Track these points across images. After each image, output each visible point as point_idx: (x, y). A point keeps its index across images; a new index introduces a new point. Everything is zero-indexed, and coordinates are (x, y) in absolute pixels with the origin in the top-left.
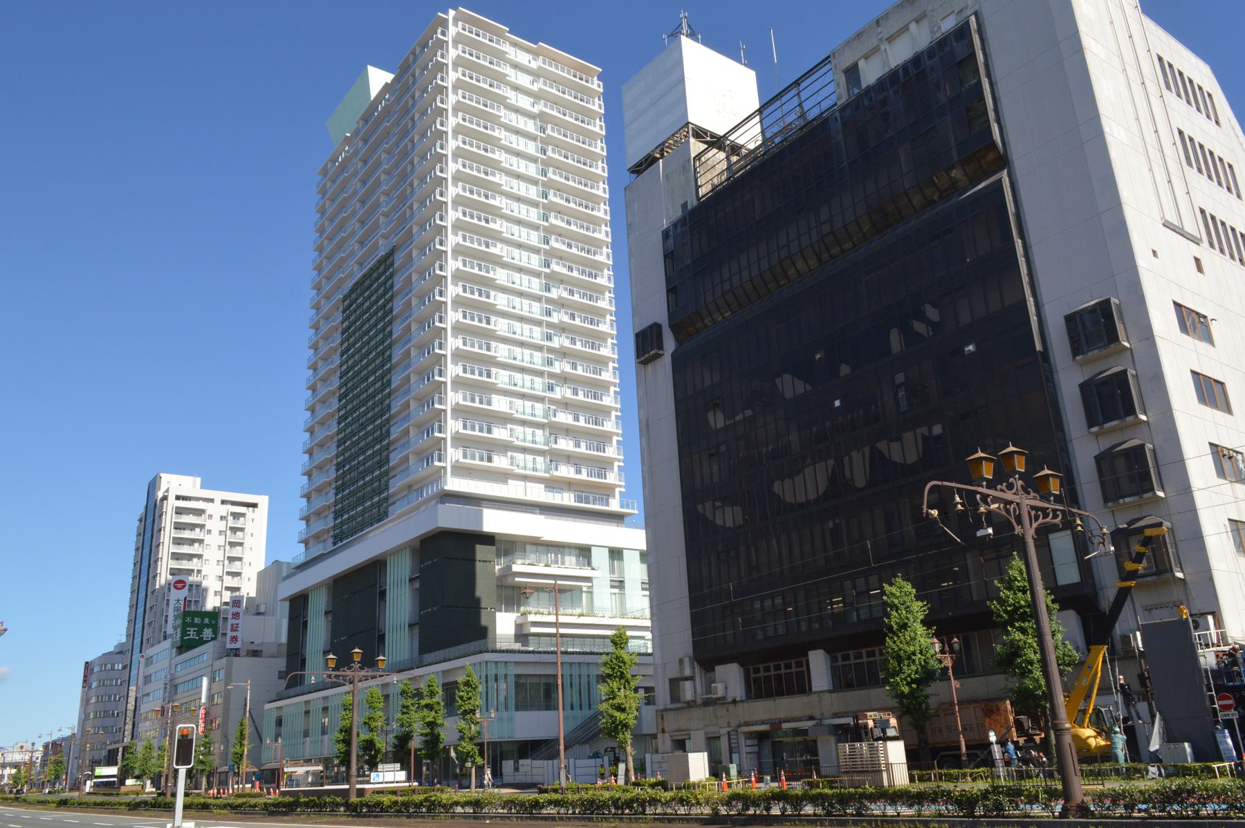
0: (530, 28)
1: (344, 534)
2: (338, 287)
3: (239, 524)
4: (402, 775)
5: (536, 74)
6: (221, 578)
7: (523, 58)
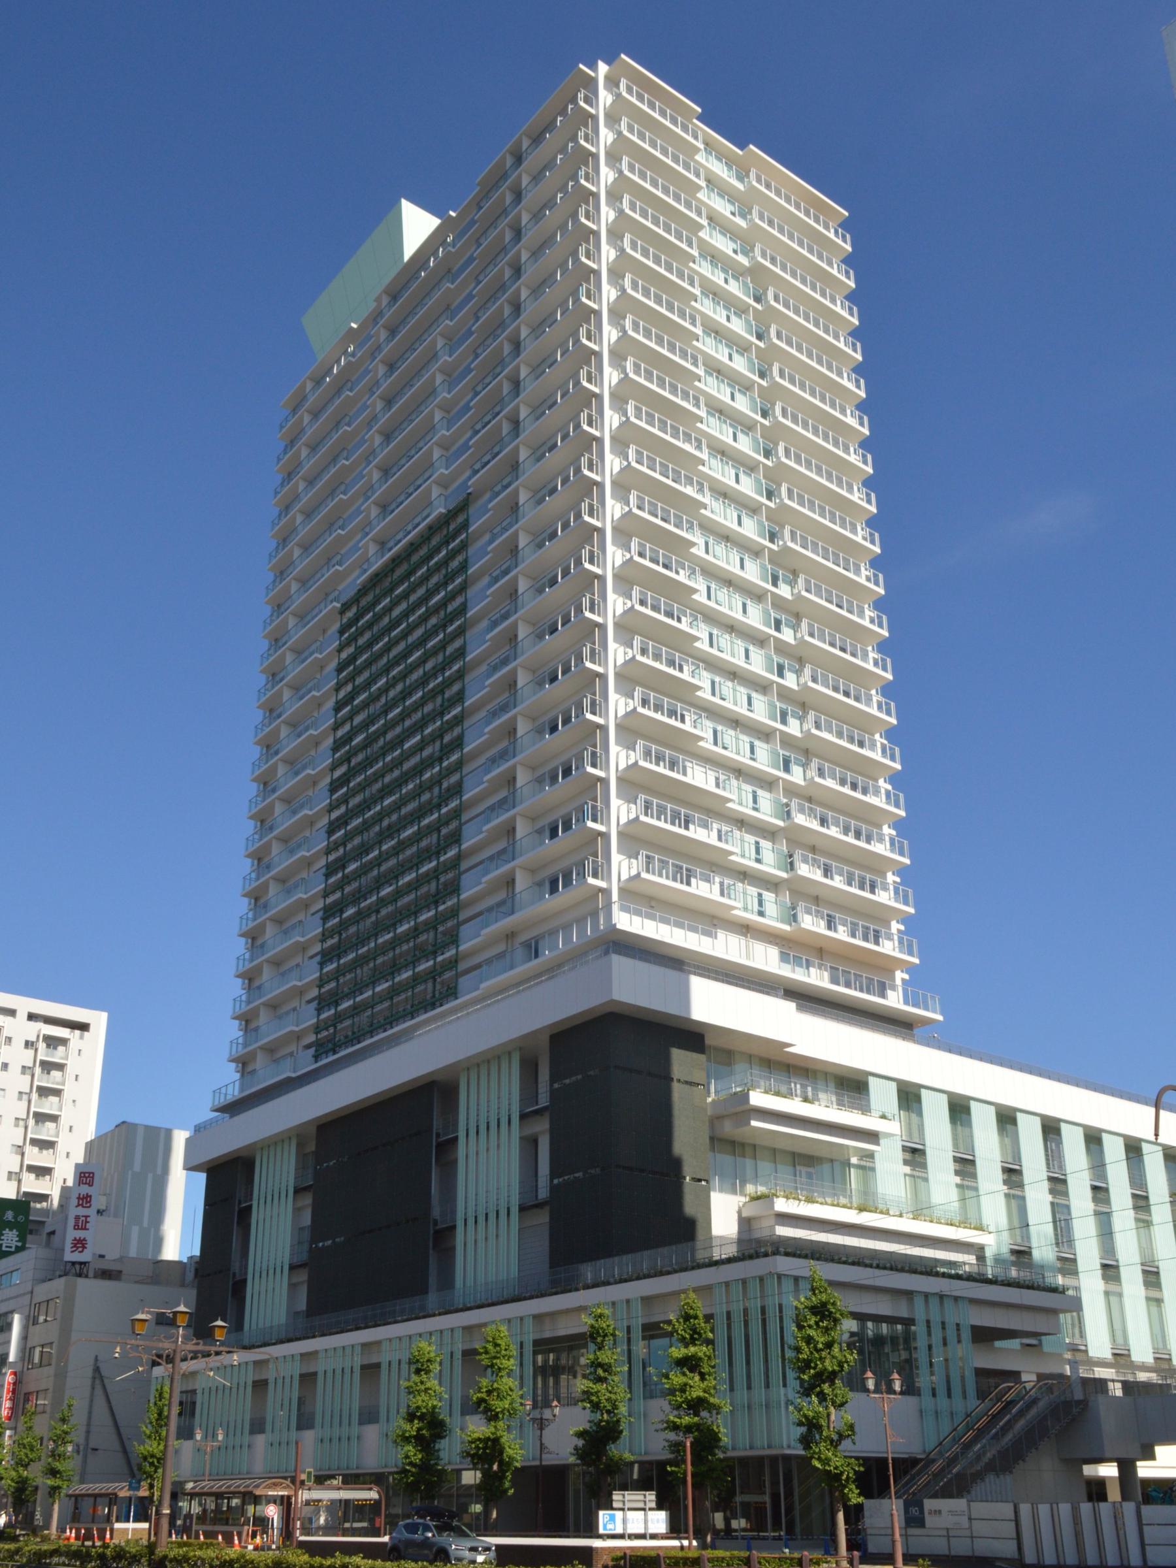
1: (334, 1044)
2: (326, 595)
3: (57, 1056)
4: (659, 1521)
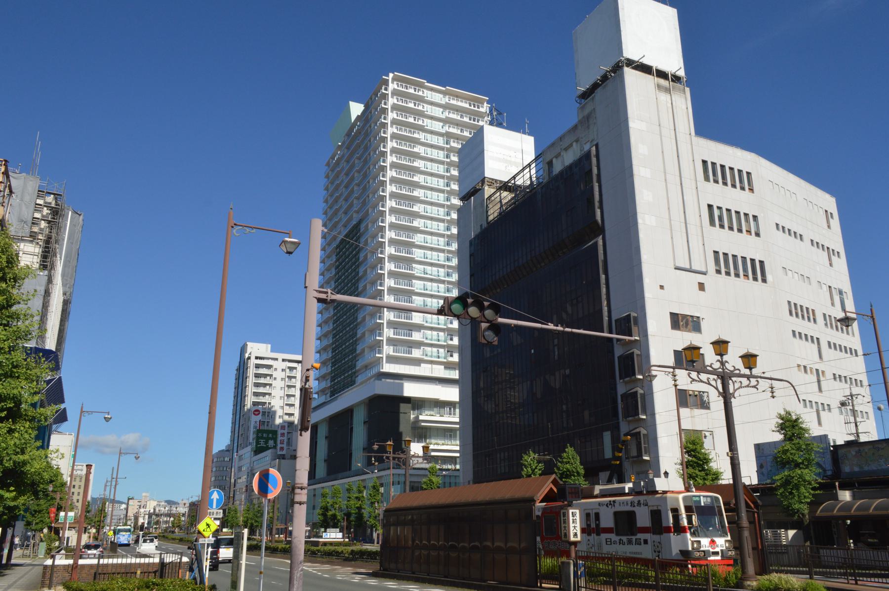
0: (441, 76)
4: (340, 535)
5: (445, 107)
6: (282, 408)
7: (438, 98)
